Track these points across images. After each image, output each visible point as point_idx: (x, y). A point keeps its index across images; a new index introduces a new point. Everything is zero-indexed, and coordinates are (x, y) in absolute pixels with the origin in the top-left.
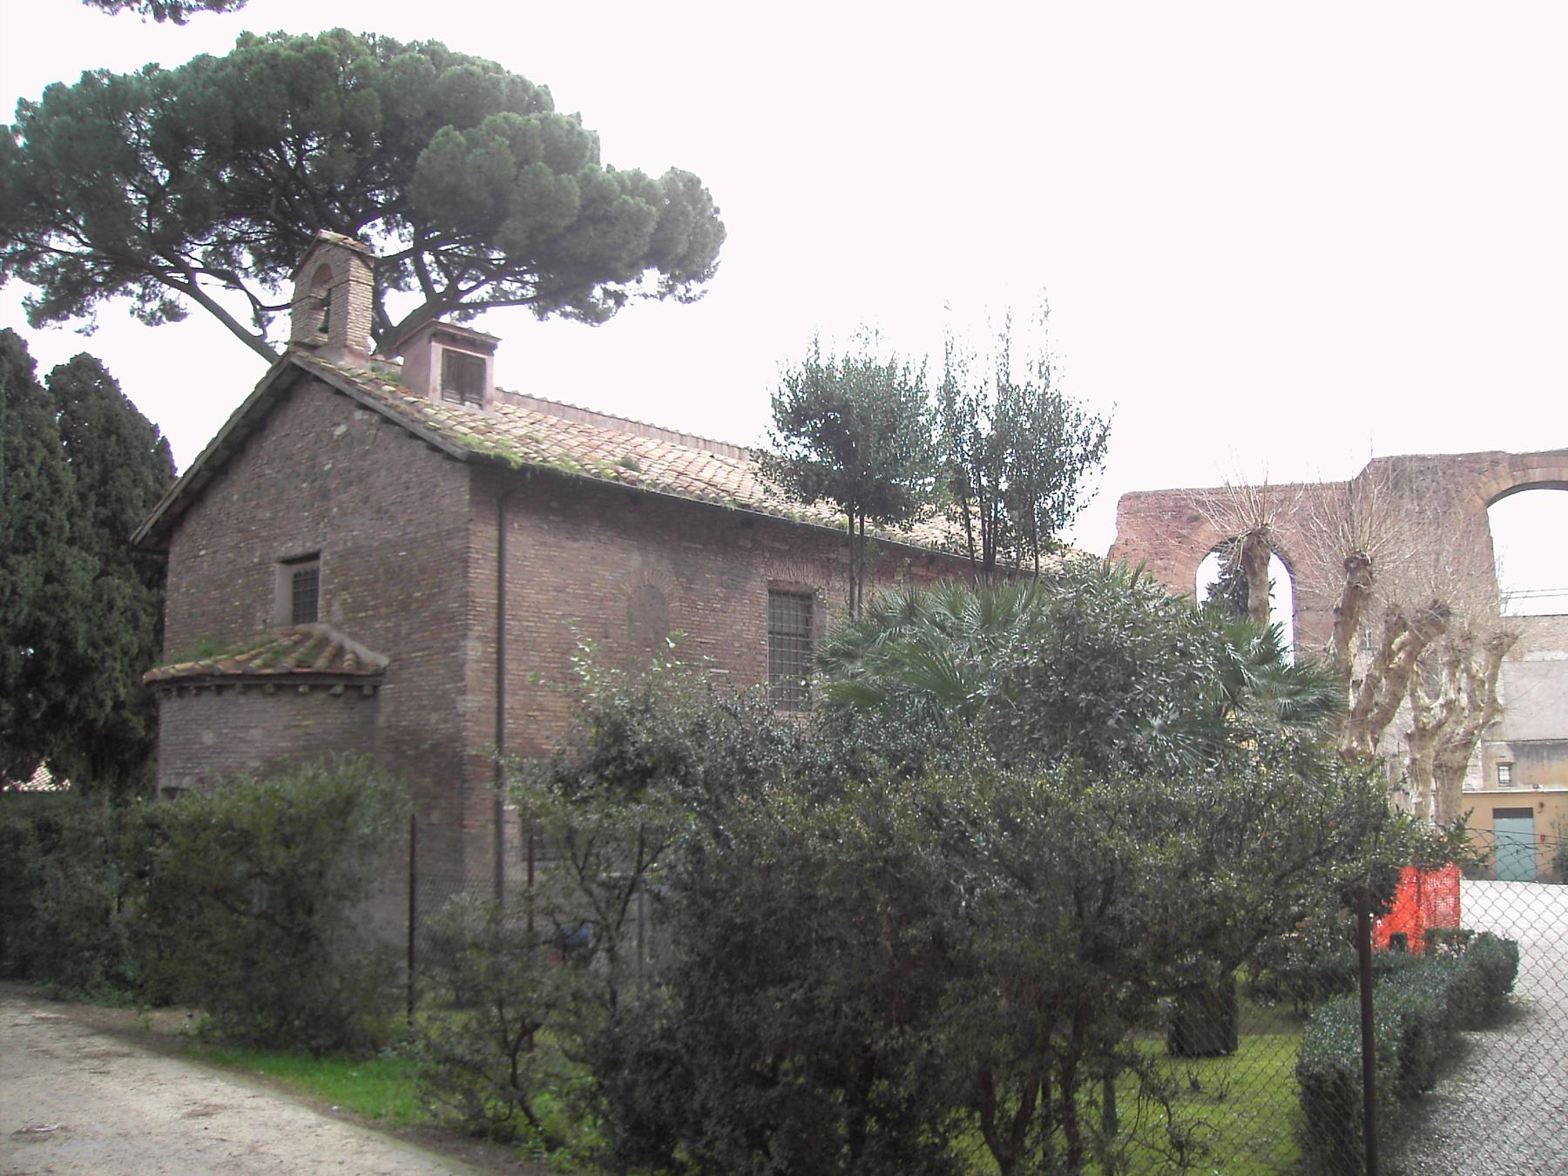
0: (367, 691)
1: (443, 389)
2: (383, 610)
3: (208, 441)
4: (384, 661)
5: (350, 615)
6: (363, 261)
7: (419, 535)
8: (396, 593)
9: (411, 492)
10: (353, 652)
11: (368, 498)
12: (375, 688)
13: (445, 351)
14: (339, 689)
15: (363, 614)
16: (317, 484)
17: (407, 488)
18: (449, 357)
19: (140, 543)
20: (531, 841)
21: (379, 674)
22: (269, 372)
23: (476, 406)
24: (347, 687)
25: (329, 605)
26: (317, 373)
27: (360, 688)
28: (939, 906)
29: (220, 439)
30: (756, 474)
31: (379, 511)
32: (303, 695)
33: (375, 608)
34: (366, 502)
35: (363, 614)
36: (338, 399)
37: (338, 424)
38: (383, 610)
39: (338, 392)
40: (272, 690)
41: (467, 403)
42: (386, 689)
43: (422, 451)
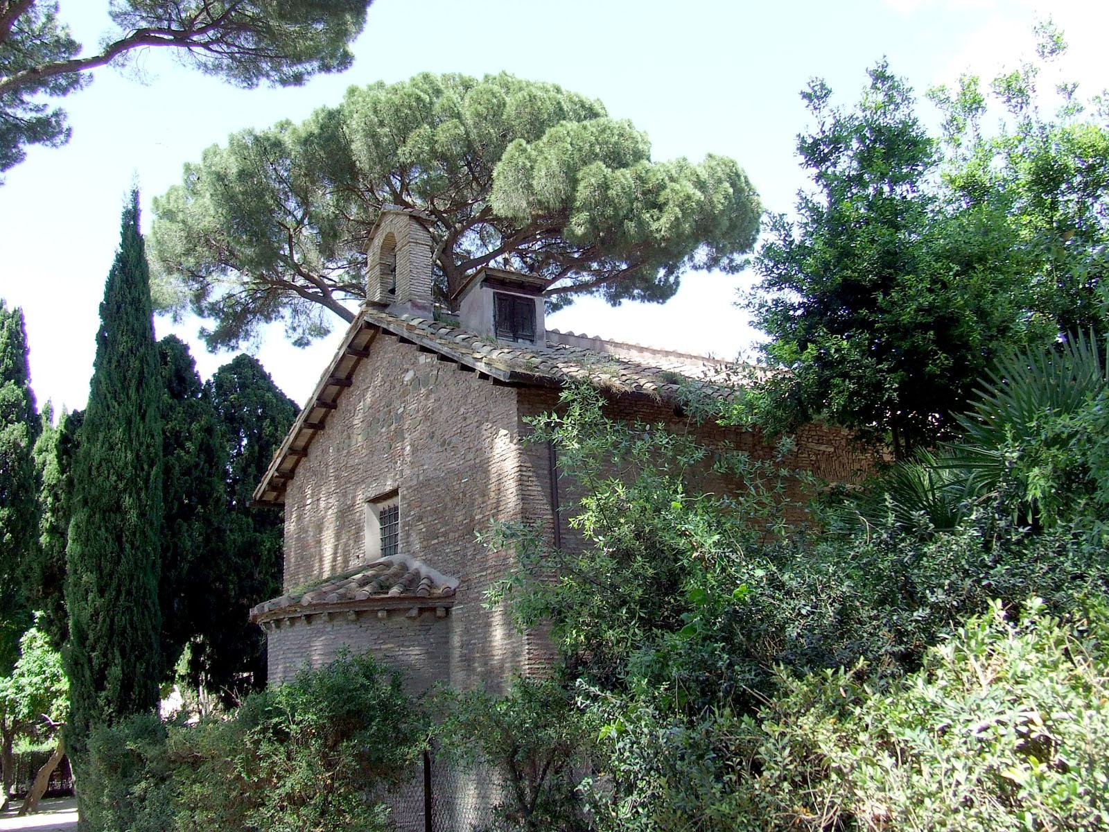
0: (440, 612)
1: (496, 329)
2: (451, 535)
3: (98, 295)
4: (453, 583)
5: (425, 543)
6: (421, 224)
7: (477, 461)
8: (459, 519)
9: (469, 422)
10: (428, 578)
11: (433, 433)
12: (448, 610)
13: (495, 293)
14: (414, 613)
15: (436, 541)
16: (393, 427)
17: (465, 419)
18: (499, 299)
19: (261, 497)
20: (796, 287)
21: (450, 595)
22: (348, 334)
23: (528, 342)
24: (421, 610)
25: (408, 535)
26: (385, 326)
27: (434, 609)
28: (510, 491)
29: (315, 398)
30: (873, 241)
31: (443, 444)
32: (380, 620)
33: (445, 534)
34: (432, 438)
35: (436, 541)
36: (405, 347)
37: (407, 370)
38: (451, 535)
39: (403, 340)
40: (353, 617)
41: (520, 340)
42: (456, 610)
43: (476, 383)
